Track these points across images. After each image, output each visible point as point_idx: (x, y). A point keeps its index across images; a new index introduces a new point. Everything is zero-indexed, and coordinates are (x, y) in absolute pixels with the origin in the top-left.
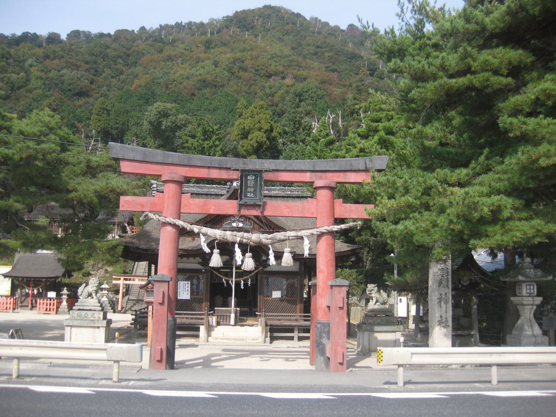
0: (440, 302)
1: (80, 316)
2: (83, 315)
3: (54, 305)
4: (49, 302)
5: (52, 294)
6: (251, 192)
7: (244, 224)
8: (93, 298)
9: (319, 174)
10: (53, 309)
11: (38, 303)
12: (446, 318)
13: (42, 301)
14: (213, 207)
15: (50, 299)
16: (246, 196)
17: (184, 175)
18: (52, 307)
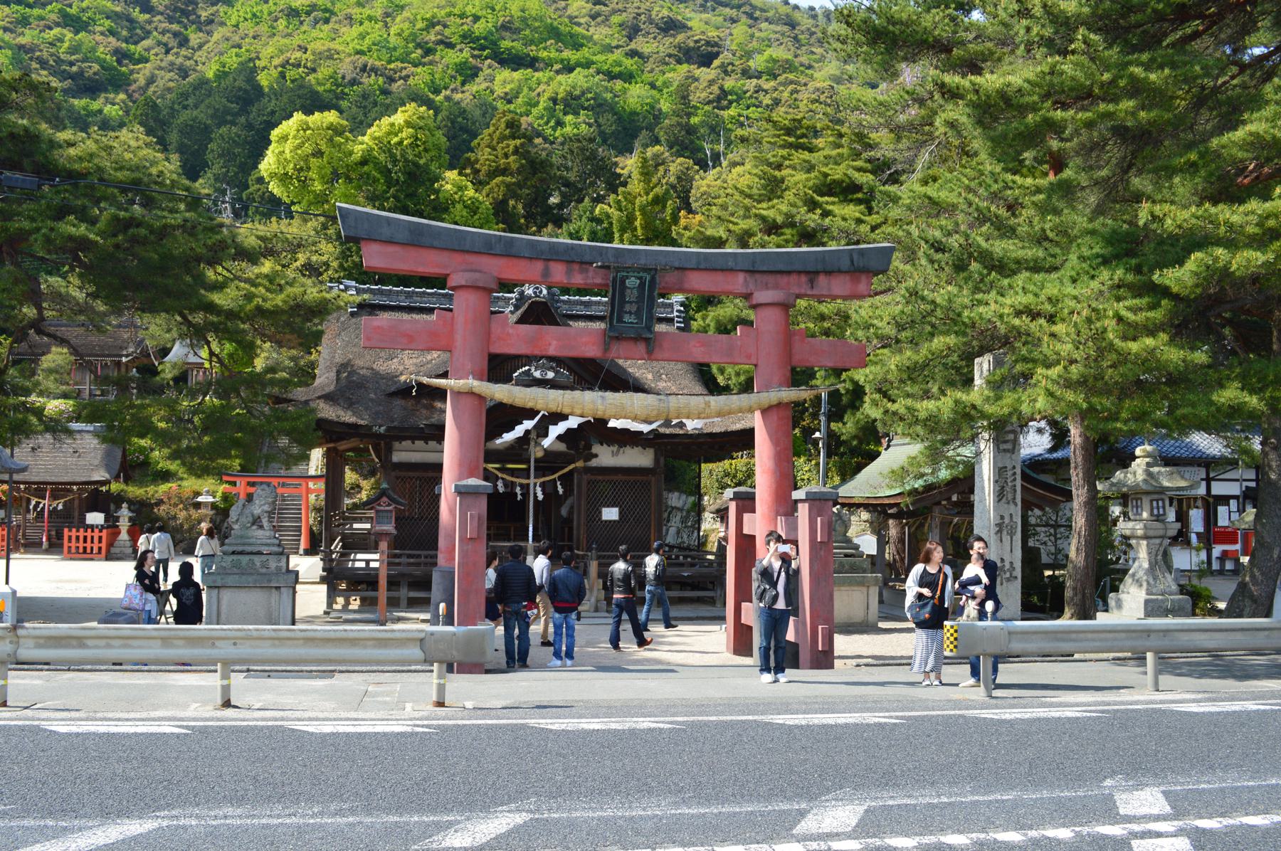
0: (1000, 532)
1: (236, 565)
2: (244, 563)
3: (100, 541)
4: (89, 534)
5: (95, 518)
6: (630, 313)
7: (557, 372)
8: (261, 527)
9: (765, 278)
10: (100, 548)
11: (66, 538)
12: (1011, 563)
13: (74, 533)
14: (554, 342)
15: (92, 527)
16: (620, 320)
17: (495, 274)
18: (88, 545)
